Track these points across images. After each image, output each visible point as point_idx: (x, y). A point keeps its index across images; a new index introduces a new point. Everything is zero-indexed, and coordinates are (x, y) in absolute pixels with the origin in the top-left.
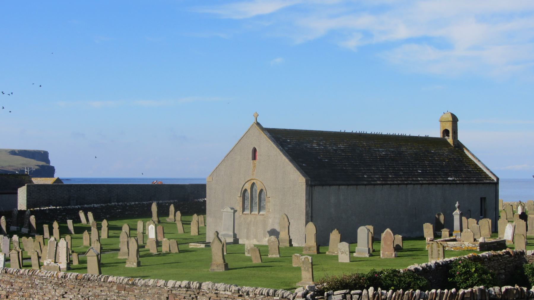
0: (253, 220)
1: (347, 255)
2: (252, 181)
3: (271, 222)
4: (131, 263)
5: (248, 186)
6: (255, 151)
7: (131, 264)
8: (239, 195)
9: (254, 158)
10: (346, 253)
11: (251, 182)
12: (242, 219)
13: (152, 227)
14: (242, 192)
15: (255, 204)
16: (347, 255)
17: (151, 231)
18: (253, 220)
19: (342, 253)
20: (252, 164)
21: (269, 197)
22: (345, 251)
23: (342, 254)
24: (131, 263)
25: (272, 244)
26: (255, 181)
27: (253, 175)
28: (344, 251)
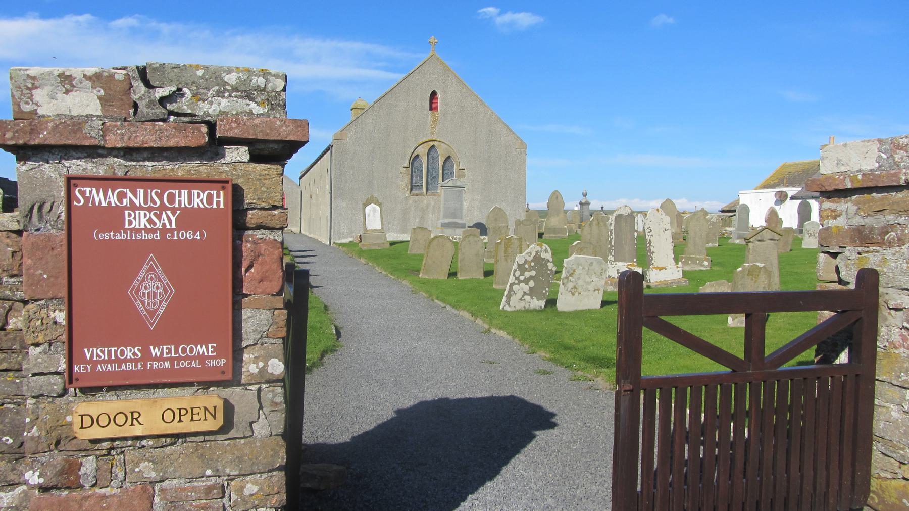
0: (433, 203)
1: (816, 238)
2: (431, 144)
3: (466, 206)
4: (698, 262)
5: (423, 151)
6: (434, 95)
7: (697, 263)
8: (406, 164)
9: (433, 106)
10: (814, 235)
11: (428, 145)
12: (411, 202)
13: (374, 209)
14: (411, 159)
15: (431, 179)
16: (816, 238)
17: (371, 215)
18: (433, 203)
19: (810, 235)
20: (430, 116)
21: (464, 169)
22: (814, 233)
23: (809, 237)
24: (698, 262)
25: (711, 226)
26: (435, 144)
27: (432, 133)
28: (812, 233)
